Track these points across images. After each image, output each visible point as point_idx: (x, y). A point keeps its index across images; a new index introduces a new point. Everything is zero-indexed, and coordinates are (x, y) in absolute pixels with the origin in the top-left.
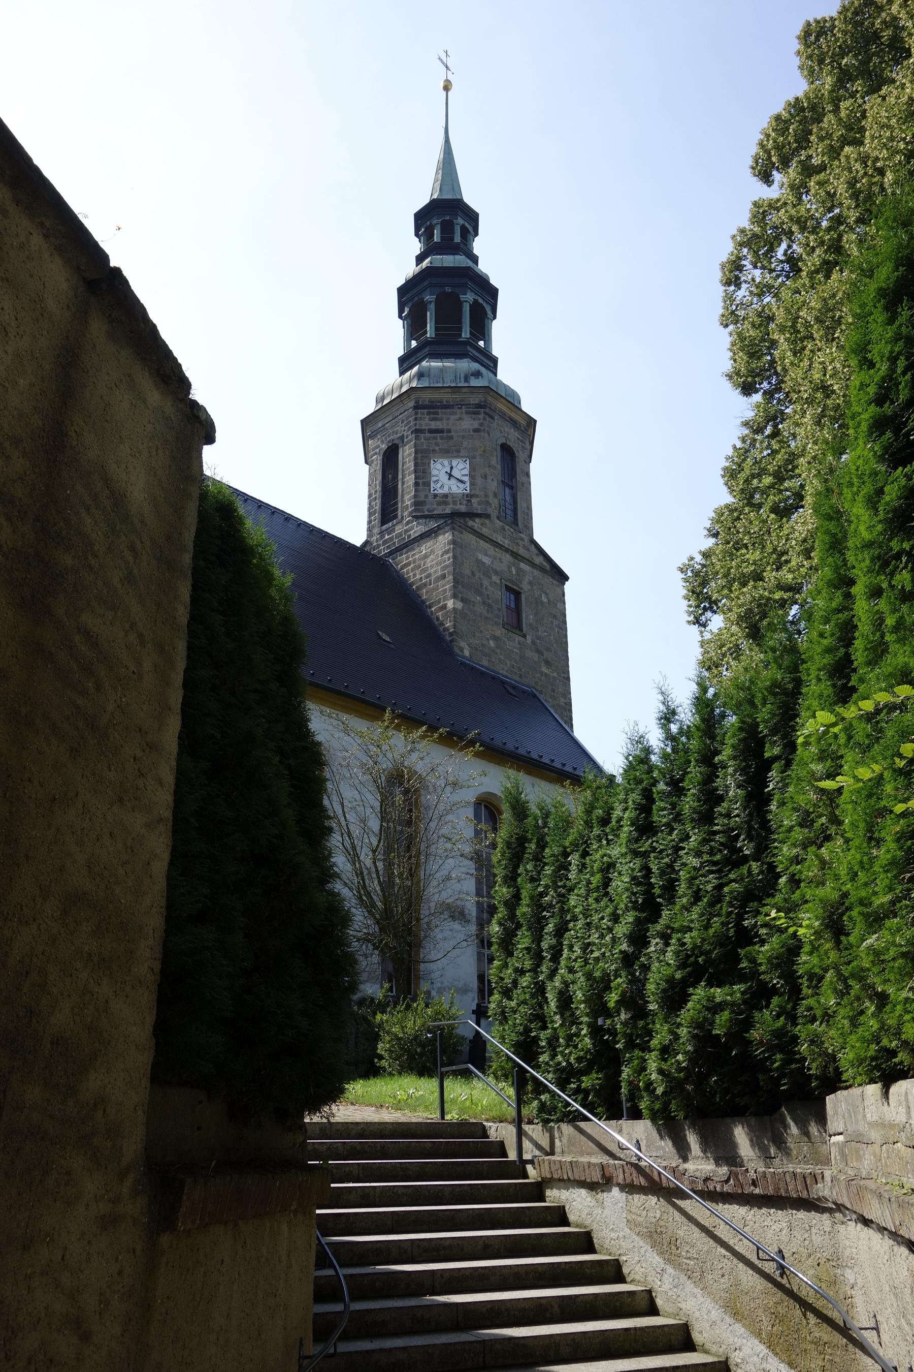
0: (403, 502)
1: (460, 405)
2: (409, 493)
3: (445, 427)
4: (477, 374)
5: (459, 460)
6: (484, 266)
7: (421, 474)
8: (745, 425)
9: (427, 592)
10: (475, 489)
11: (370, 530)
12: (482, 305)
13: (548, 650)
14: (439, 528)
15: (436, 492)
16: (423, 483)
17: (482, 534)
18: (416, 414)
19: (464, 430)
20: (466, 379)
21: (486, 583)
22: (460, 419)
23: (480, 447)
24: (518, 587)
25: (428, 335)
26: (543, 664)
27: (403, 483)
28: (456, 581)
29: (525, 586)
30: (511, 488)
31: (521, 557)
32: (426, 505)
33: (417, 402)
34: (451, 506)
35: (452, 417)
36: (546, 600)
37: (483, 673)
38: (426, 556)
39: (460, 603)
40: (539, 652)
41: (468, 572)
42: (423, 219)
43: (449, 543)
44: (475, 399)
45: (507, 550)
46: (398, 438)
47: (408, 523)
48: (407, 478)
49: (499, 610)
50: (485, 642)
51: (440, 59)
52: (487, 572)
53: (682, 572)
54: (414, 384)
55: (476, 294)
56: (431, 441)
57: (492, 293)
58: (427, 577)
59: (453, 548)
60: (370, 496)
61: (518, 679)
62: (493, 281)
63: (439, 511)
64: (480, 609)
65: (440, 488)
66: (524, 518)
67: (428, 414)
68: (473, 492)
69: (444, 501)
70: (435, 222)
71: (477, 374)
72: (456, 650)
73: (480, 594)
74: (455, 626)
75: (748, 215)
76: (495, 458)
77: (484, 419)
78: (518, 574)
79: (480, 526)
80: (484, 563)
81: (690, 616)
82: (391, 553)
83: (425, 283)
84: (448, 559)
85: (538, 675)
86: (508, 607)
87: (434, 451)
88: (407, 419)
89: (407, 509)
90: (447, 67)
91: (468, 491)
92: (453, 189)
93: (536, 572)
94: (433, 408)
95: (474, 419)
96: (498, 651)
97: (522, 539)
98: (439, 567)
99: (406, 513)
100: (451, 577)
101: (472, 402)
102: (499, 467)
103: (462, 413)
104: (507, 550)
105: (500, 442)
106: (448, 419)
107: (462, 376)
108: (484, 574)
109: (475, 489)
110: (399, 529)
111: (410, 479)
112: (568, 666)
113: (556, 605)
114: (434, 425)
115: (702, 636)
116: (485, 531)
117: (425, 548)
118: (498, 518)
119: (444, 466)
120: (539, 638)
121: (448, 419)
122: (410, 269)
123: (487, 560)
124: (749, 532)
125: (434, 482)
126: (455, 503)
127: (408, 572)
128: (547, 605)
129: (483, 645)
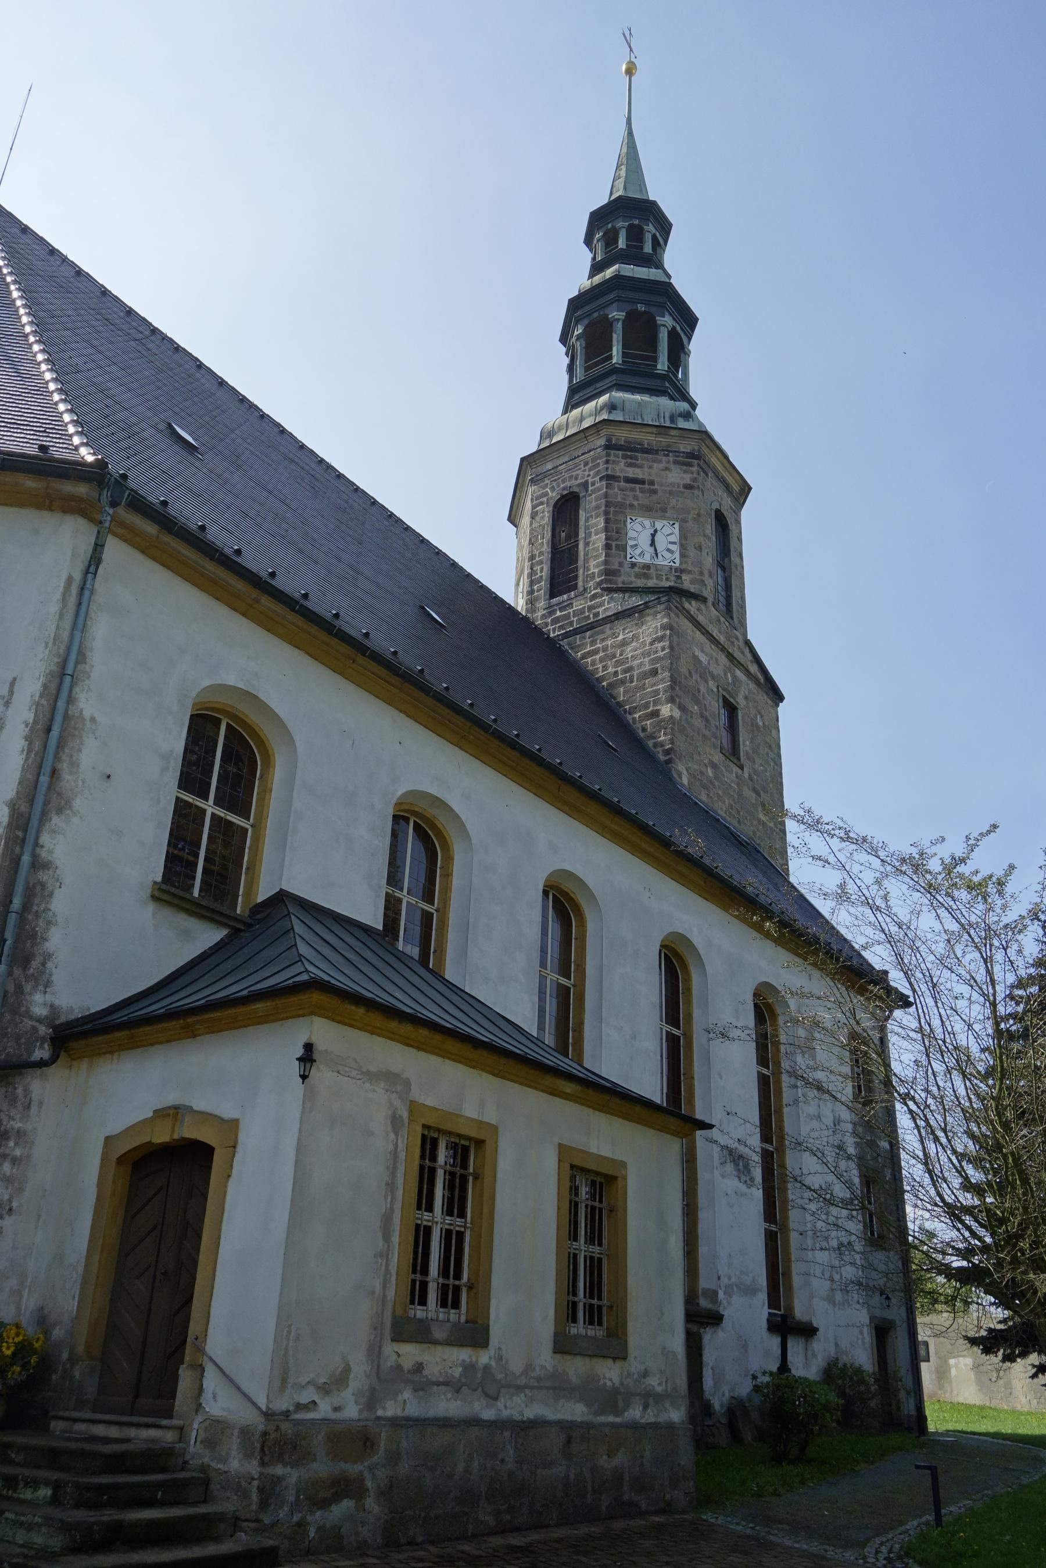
1: (667, 451)
2: (596, 557)
3: (646, 477)
5: (665, 522)
7: (614, 534)
10: (686, 562)
13: (766, 792)
15: (633, 560)
16: (617, 546)
18: (608, 455)
19: (672, 485)
21: (703, 689)
22: (666, 469)
23: (693, 509)
24: (735, 700)
25: (614, 361)
27: (587, 544)
28: (673, 680)
29: (740, 701)
30: (724, 569)
32: (620, 576)
33: (609, 440)
35: (655, 465)
36: (761, 724)
38: (624, 643)
39: (677, 711)
44: (686, 446)
45: (723, 649)
46: (578, 485)
47: (594, 597)
48: (594, 537)
50: (703, 769)
51: (624, 34)
52: (704, 674)
55: (674, 319)
56: (627, 493)
57: (688, 320)
58: (625, 671)
64: (698, 723)
65: (640, 555)
67: (625, 457)
68: (684, 566)
69: (645, 574)
70: (620, 224)
72: (675, 775)
73: (697, 702)
74: (672, 742)
78: (734, 683)
79: (696, 612)
80: (700, 662)
83: (611, 296)
84: (662, 649)
87: (632, 506)
90: (631, 50)
91: (678, 565)
95: (685, 472)
98: (647, 659)
100: (667, 674)
101: (682, 450)
102: (714, 538)
103: (668, 462)
104: (723, 649)
109: (686, 562)
110: (578, 605)
111: (599, 540)
113: (771, 732)
114: (631, 472)
116: (701, 618)
117: (622, 632)
120: (756, 772)
121: (650, 467)
123: (703, 658)
125: (632, 546)
126: (659, 577)
128: (762, 729)
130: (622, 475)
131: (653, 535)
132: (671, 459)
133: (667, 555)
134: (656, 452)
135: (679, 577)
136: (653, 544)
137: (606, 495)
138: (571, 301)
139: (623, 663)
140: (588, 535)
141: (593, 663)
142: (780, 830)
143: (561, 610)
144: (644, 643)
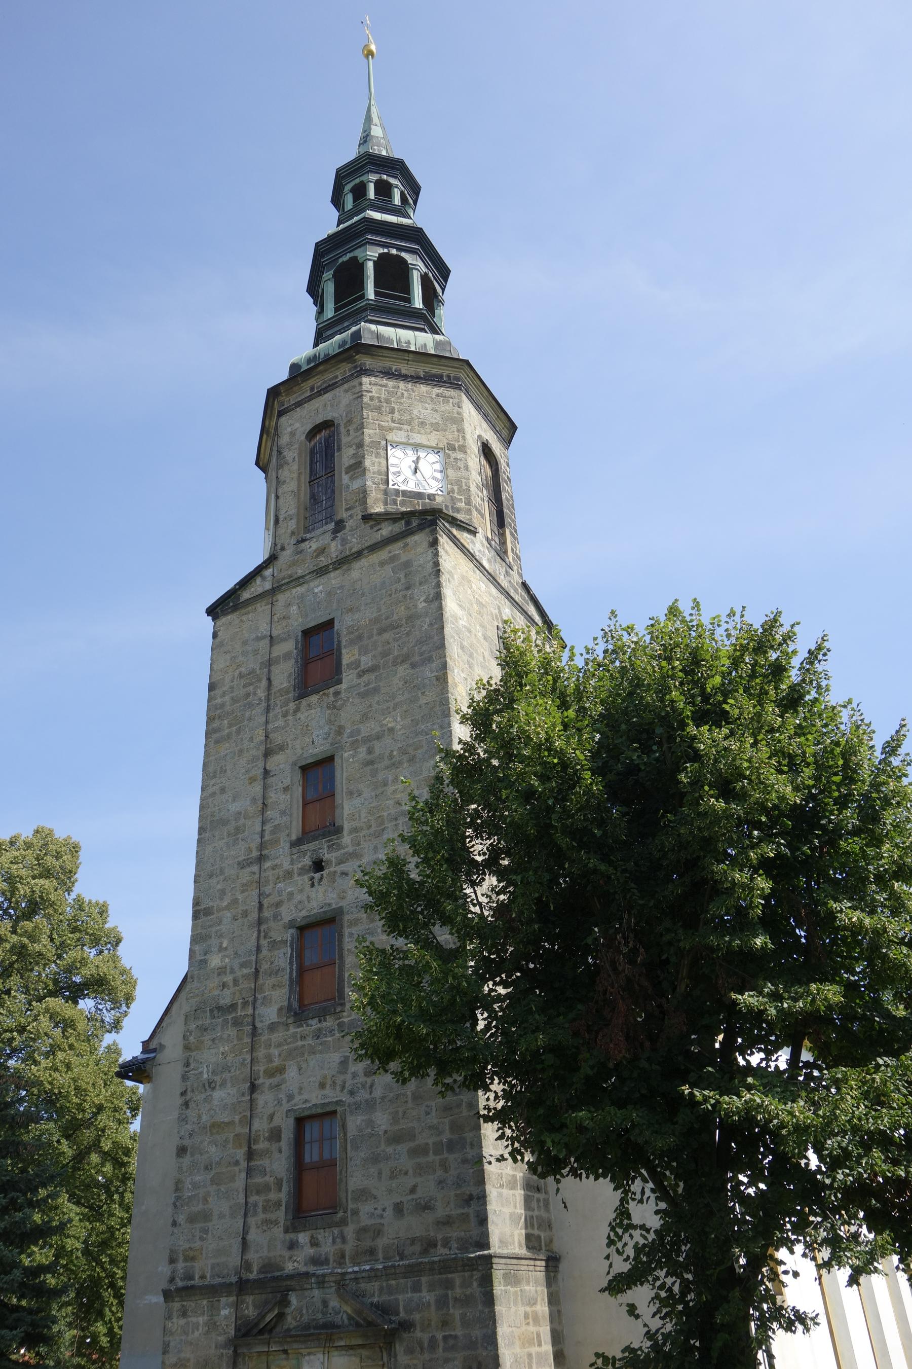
65: (403, 482)
125: (395, 473)
138: (332, 201)
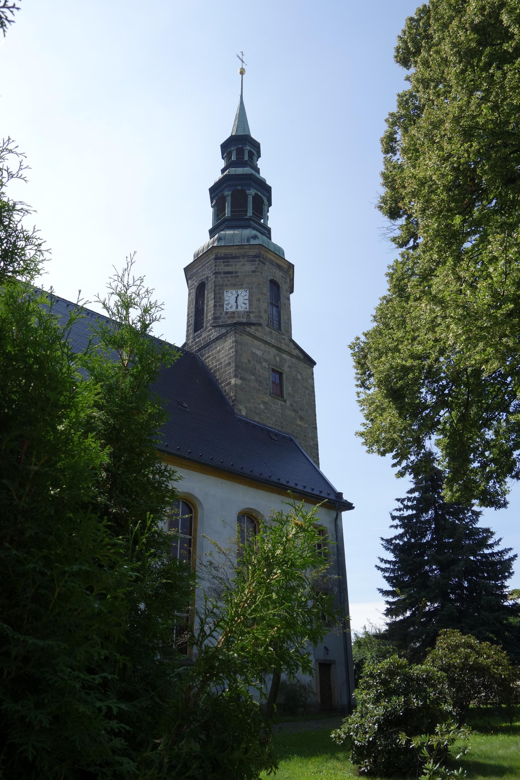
0: (207, 317)
1: (244, 256)
2: (211, 312)
3: (234, 270)
4: (255, 237)
5: (243, 290)
6: (263, 174)
8: (393, 241)
9: (219, 374)
10: (252, 308)
11: (187, 336)
12: (260, 197)
14: (227, 333)
16: (219, 305)
17: (256, 336)
18: (216, 262)
20: (248, 240)
21: (258, 367)
22: (243, 265)
26: (298, 419)
27: (207, 306)
28: (237, 367)
29: (286, 369)
30: (277, 307)
31: (283, 350)
34: (237, 319)
35: (238, 264)
37: (254, 426)
38: (219, 351)
39: (239, 380)
40: (296, 411)
41: (245, 360)
42: (226, 147)
43: (233, 342)
44: (253, 252)
45: (273, 346)
48: (210, 302)
49: (267, 384)
51: (238, 56)
53: (352, 349)
54: (215, 245)
57: (268, 190)
59: (236, 345)
60: (188, 315)
61: (280, 429)
62: (268, 183)
63: (230, 322)
66: (285, 326)
67: (223, 262)
68: (251, 310)
71: (255, 237)
72: (236, 411)
74: (235, 396)
75: (396, 104)
76: (266, 289)
77: (259, 264)
79: (254, 331)
80: (257, 355)
81: (358, 381)
82: (199, 350)
85: (294, 426)
86: (274, 383)
87: (227, 285)
88: (211, 266)
89: (209, 322)
90: (242, 61)
92: (244, 130)
93: (294, 360)
94: (227, 258)
95: (252, 265)
96: (266, 411)
97: (284, 339)
99: (209, 324)
100: (234, 364)
102: (269, 294)
104: (273, 346)
105: (269, 279)
106: (236, 265)
107: (246, 239)
108: (257, 362)
109: (252, 308)
111: (211, 303)
112: (316, 420)
113: (307, 381)
114: (227, 269)
115: (359, 397)
116: (258, 334)
118: (267, 326)
119: (232, 294)
122: (218, 176)
123: (259, 353)
124: (394, 316)
126: (239, 317)
127: (209, 362)
129: (255, 407)
130: (222, 271)
131: (237, 298)
132: (246, 260)
133: (244, 306)
134: (238, 257)
135: (248, 316)
136: (236, 302)
137: (215, 282)
139: (219, 361)
140: (208, 302)
141: (208, 361)
142: (312, 427)
143: (198, 338)
144: (226, 350)
